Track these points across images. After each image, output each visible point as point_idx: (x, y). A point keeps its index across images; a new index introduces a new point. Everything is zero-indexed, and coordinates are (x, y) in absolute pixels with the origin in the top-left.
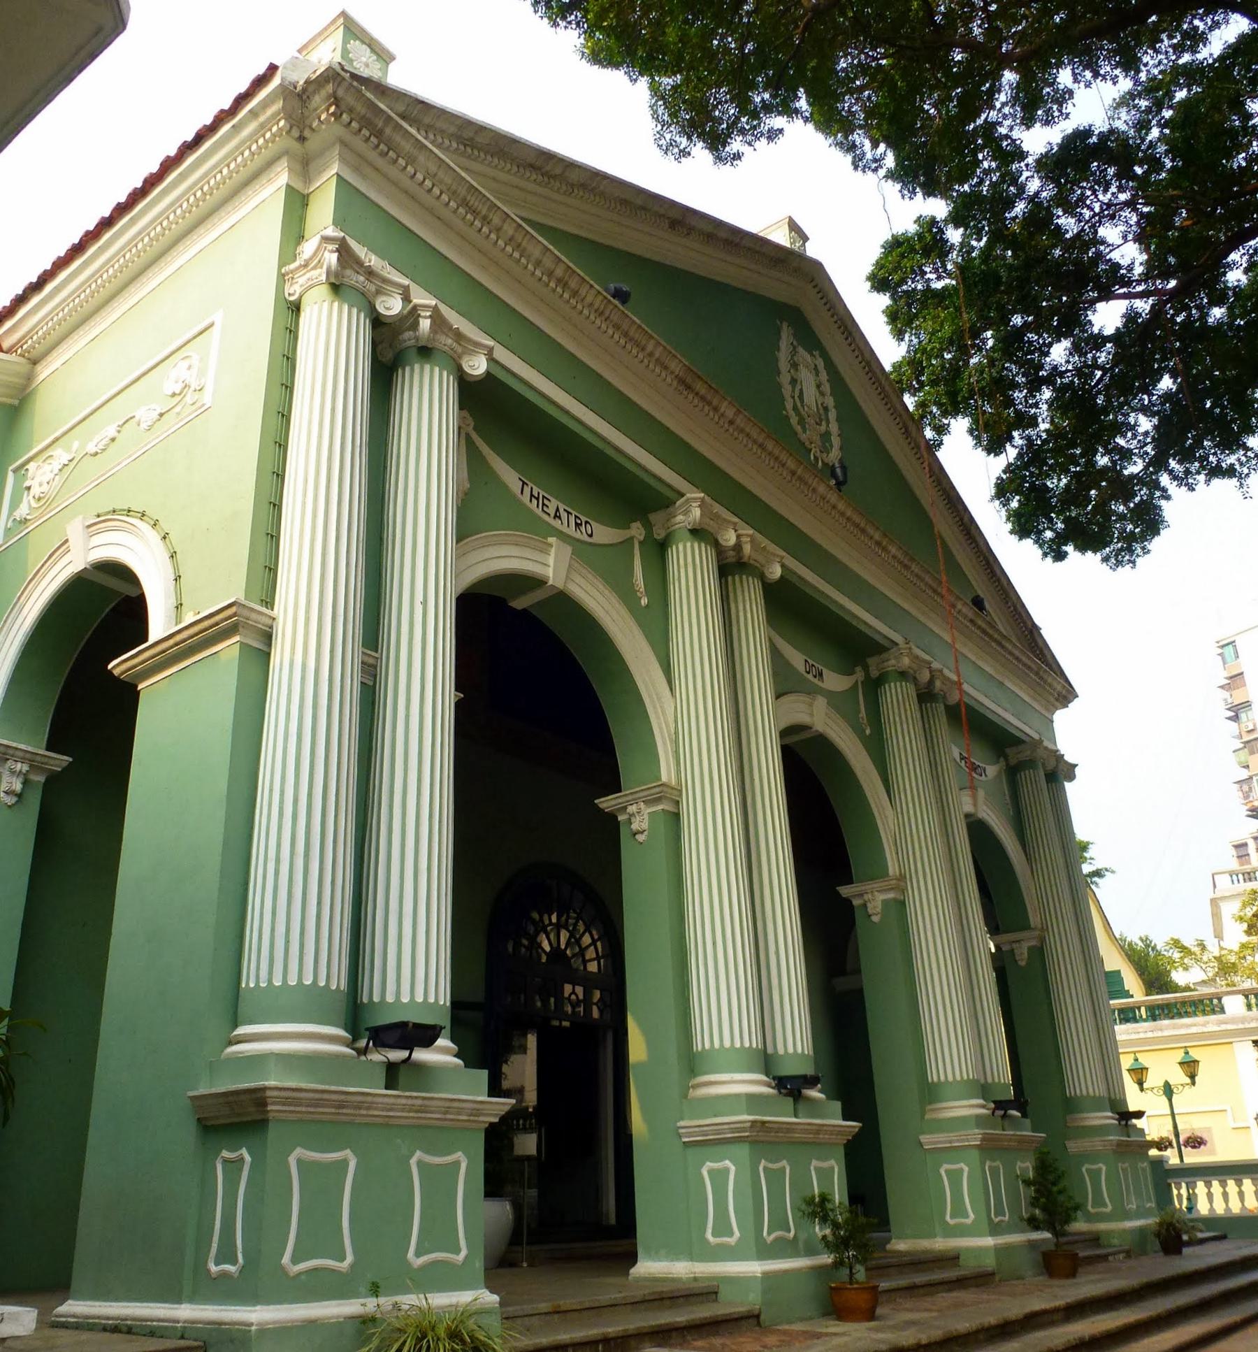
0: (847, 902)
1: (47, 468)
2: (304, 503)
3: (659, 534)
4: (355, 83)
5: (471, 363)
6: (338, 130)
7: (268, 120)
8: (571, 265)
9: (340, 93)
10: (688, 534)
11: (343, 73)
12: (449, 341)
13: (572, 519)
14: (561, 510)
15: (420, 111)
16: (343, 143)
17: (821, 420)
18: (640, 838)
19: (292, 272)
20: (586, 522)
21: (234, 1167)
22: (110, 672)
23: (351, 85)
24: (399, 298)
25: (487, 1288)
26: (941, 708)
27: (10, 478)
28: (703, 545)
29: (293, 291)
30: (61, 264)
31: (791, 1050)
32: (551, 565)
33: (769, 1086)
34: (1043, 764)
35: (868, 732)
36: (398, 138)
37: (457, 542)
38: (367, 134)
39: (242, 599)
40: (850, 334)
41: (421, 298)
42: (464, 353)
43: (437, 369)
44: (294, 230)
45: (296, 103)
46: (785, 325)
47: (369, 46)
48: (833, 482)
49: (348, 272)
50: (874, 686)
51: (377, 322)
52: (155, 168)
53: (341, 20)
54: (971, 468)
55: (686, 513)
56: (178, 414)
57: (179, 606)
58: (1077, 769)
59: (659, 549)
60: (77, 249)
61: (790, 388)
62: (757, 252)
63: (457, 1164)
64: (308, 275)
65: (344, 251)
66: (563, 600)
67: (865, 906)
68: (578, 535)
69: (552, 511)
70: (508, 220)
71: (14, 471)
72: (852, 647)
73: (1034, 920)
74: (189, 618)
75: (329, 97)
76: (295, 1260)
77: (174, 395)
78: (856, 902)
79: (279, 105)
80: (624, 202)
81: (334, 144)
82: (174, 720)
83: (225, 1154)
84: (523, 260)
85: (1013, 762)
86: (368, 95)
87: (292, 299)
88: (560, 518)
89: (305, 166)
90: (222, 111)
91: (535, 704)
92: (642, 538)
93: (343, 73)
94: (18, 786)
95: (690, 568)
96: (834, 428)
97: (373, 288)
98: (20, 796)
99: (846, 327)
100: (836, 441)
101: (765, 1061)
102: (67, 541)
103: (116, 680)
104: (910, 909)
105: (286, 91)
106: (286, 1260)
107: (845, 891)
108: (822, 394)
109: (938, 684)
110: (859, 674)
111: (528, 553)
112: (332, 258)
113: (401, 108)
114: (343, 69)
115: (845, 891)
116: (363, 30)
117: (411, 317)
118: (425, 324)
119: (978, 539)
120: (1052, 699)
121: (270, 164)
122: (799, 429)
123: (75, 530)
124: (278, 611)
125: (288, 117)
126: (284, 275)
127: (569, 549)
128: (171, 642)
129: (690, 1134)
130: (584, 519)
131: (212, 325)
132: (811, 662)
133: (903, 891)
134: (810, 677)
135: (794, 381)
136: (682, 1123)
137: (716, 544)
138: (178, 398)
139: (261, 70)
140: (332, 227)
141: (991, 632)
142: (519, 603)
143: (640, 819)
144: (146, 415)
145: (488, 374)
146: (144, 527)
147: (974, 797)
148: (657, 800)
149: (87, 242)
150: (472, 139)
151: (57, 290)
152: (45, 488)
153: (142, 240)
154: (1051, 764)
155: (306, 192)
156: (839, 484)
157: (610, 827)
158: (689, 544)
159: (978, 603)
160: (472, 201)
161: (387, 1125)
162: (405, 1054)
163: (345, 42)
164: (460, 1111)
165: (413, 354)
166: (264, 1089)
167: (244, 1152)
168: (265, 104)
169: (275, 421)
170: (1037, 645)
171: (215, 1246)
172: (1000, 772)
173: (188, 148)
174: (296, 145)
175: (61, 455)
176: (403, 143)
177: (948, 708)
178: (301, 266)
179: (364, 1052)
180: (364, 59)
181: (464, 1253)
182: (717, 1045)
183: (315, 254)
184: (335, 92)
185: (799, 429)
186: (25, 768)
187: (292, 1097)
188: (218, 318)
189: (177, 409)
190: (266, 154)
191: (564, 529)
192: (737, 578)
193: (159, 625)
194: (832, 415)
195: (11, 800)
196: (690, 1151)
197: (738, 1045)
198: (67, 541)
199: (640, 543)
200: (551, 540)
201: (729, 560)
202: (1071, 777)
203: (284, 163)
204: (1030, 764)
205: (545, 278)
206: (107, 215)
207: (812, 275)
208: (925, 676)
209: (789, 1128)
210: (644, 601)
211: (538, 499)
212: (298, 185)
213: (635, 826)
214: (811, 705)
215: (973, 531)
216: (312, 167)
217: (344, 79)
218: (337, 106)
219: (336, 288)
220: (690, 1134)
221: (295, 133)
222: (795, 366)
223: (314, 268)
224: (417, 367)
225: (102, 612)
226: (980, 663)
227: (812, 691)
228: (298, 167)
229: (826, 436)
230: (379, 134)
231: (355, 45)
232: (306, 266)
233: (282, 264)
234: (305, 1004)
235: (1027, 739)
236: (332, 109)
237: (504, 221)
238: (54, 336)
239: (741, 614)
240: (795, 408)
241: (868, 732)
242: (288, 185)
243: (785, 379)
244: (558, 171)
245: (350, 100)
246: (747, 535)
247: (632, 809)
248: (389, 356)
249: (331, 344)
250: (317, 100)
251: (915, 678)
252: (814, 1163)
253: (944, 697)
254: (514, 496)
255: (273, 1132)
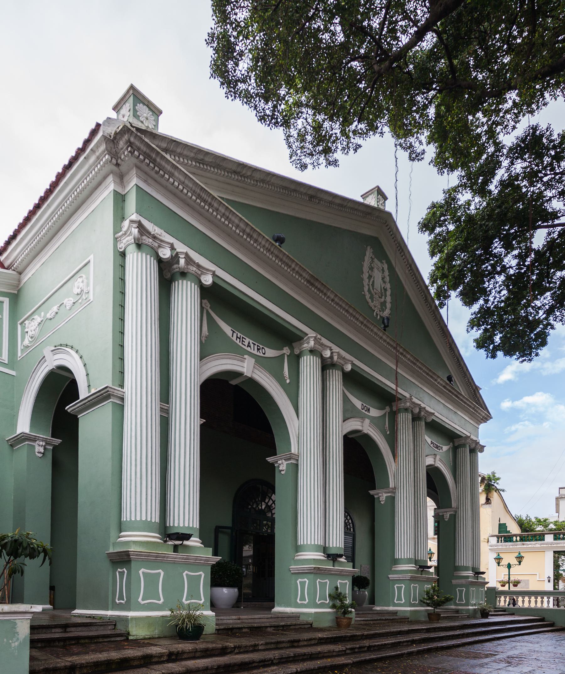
0: (373, 496)
1: (32, 323)
2: (132, 346)
3: (297, 352)
4: (139, 134)
5: (205, 279)
6: (134, 160)
7: (101, 154)
8: (253, 226)
9: (132, 139)
10: (308, 353)
11: (132, 129)
12: (195, 269)
13: (256, 347)
14: (251, 343)
15: (174, 146)
16: (138, 167)
17: (382, 295)
18: (283, 473)
19: (120, 237)
20: (263, 348)
21: (122, 574)
22: (66, 411)
23: (136, 135)
24: (169, 249)
25: (211, 610)
26: (424, 423)
27: (19, 326)
28: (315, 357)
29: (121, 246)
30: (22, 226)
31: (335, 546)
32: (246, 367)
33: (324, 557)
34: (469, 446)
35: (388, 433)
36: (163, 163)
37: (201, 360)
38: (148, 162)
39: (111, 386)
40: (403, 250)
41: (181, 248)
42: (201, 274)
43: (189, 283)
44: (120, 215)
45: (111, 145)
46: (369, 248)
47: (148, 106)
48: (383, 326)
49: (144, 237)
50: (393, 416)
51: (160, 261)
52: (54, 179)
53: (131, 92)
54: (457, 315)
55: (308, 343)
56: (81, 303)
57: (89, 386)
58: (485, 448)
59: (296, 360)
60: (27, 220)
61: (367, 280)
62: (356, 210)
63: (201, 575)
64: (127, 239)
65: (140, 226)
66: (251, 381)
67: (379, 498)
68: (258, 354)
69: (246, 344)
70: (222, 205)
71: (21, 324)
72: (385, 399)
73: (454, 504)
74: (93, 391)
75: (127, 143)
76: (143, 600)
77: (78, 294)
78: (376, 497)
79: (103, 147)
80: (285, 188)
81: (132, 168)
82: (93, 428)
83: (119, 570)
84: (230, 225)
85: (456, 444)
86: (146, 140)
87: (121, 250)
88: (250, 346)
89: (121, 178)
90: (79, 149)
91: (237, 425)
92: (288, 354)
93: (132, 129)
94: (42, 451)
95: (309, 367)
96: (389, 299)
97: (156, 245)
98: (43, 454)
99: (401, 247)
100: (388, 305)
101: (325, 549)
102: (44, 357)
103: (69, 413)
104: (396, 499)
105: (105, 138)
106: (140, 600)
107: (372, 492)
108: (384, 282)
109: (423, 413)
110: (388, 409)
111: (235, 362)
112: (135, 231)
113: (164, 145)
114: (131, 126)
115: (372, 492)
116: (144, 97)
117: (175, 258)
118: (182, 261)
119: (455, 349)
120: (480, 420)
121: (105, 178)
122: (370, 301)
123: (47, 351)
124: (125, 390)
125: (110, 153)
126: (117, 238)
127: (253, 360)
128: (87, 401)
129: (293, 570)
130: (261, 346)
131: (89, 262)
132: (365, 405)
133: (395, 493)
134: (364, 411)
135: (370, 277)
136: (291, 567)
137: (322, 357)
138: (80, 296)
139: (93, 126)
140: (135, 214)
141: (453, 391)
142: (234, 382)
143: (283, 465)
144: (68, 302)
145: (214, 282)
146: (73, 352)
147: (435, 459)
148: (290, 459)
149: (31, 216)
150: (202, 160)
151: (22, 239)
152: (33, 332)
153: (57, 213)
154: (473, 446)
155: (123, 193)
156: (386, 327)
157: (272, 468)
158: (308, 357)
159: (450, 378)
160: (204, 195)
161: (174, 563)
162: (181, 542)
163: (135, 105)
164: (201, 560)
165: (178, 275)
166: (129, 551)
167: (124, 569)
168: (97, 146)
169: (119, 309)
170: (476, 396)
171: (117, 595)
172: (449, 449)
173: (67, 168)
174: (115, 168)
175: (38, 319)
176: (166, 166)
177: (426, 423)
178: (123, 234)
179: (165, 541)
180: (145, 115)
181: (203, 600)
182: (305, 543)
183: (128, 229)
184: (129, 140)
185: (370, 301)
186: (44, 444)
187: (139, 554)
188: (91, 258)
189: (80, 301)
190: (103, 173)
191: (252, 351)
192: (331, 371)
193: (83, 393)
194: (389, 293)
195: (40, 455)
196: (293, 576)
197: (313, 543)
198: (44, 357)
199: (288, 356)
200: (246, 356)
201: (328, 363)
202: (482, 450)
203: (110, 178)
204: (464, 445)
205: (241, 234)
206: (37, 202)
207: (383, 221)
208: (417, 410)
209: (330, 570)
210: (288, 381)
211: (240, 338)
212: (119, 190)
213: (281, 468)
214: (363, 422)
215: (453, 346)
216: (125, 179)
217: (133, 132)
218: (132, 147)
219: (139, 246)
220: (293, 570)
221: (114, 161)
222: (371, 269)
223: (129, 236)
224: (180, 281)
225: (59, 390)
226: (446, 404)
227: (362, 417)
228: (118, 180)
229: (384, 304)
230: (154, 161)
231: (140, 106)
232: (125, 234)
233: (115, 233)
234: (146, 526)
235: (464, 436)
236: (129, 149)
237: (220, 205)
238: (25, 263)
239: (331, 386)
240: (369, 290)
241: (388, 433)
242: (114, 190)
243: (365, 276)
244: (249, 173)
245: (138, 143)
246: (336, 352)
247: (280, 462)
248: (167, 275)
249: (140, 272)
250: (122, 144)
251: (412, 411)
252: (339, 581)
253: (425, 419)
254: (229, 337)
255: (133, 564)
